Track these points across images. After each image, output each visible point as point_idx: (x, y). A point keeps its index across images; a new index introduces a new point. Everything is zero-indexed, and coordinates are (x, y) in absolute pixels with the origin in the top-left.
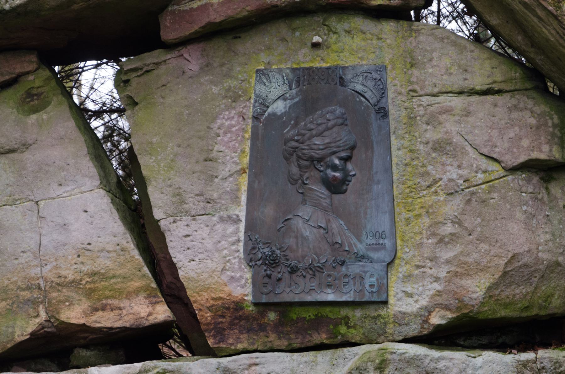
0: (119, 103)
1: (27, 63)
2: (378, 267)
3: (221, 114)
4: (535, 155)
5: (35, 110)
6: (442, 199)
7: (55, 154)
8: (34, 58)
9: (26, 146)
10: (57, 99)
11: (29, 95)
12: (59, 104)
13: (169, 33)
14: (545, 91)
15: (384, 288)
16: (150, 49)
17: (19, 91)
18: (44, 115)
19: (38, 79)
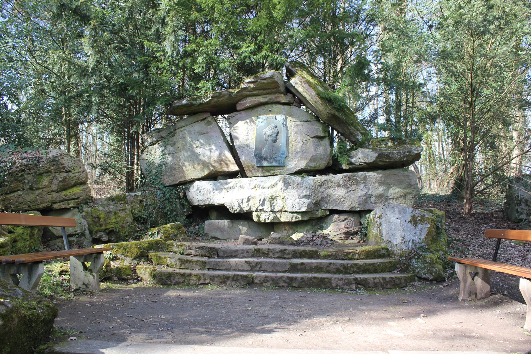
0: (410, 129)
1: (208, 114)
2: (283, 159)
3: (474, 141)
4: (317, 135)
5: (210, 125)
6: (502, 196)
7: (214, 134)
8: (209, 114)
9: (208, 133)
10: (214, 123)
11: (208, 121)
12: (154, 277)
13: (238, 108)
14: (319, 121)
15: (284, 163)
16: (234, 112)
17: (206, 121)
18: (211, 126)
19: (210, 119)
